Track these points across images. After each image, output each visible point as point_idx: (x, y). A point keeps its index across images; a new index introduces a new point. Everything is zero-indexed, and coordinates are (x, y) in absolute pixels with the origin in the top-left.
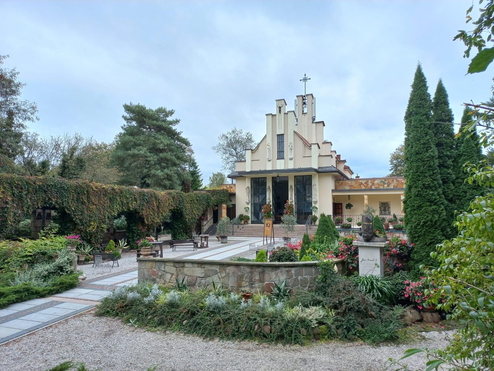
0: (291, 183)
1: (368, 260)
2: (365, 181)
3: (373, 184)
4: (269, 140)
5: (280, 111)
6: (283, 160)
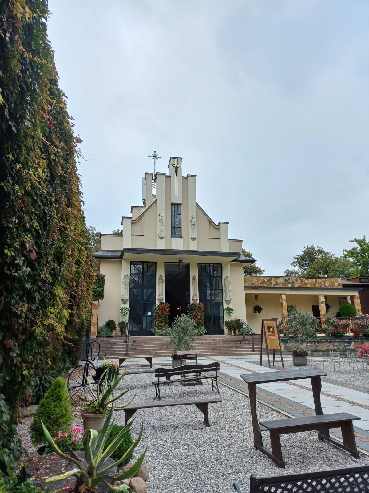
0: (194, 273)
2: (268, 279)
3: (277, 283)
5: (176, 172)
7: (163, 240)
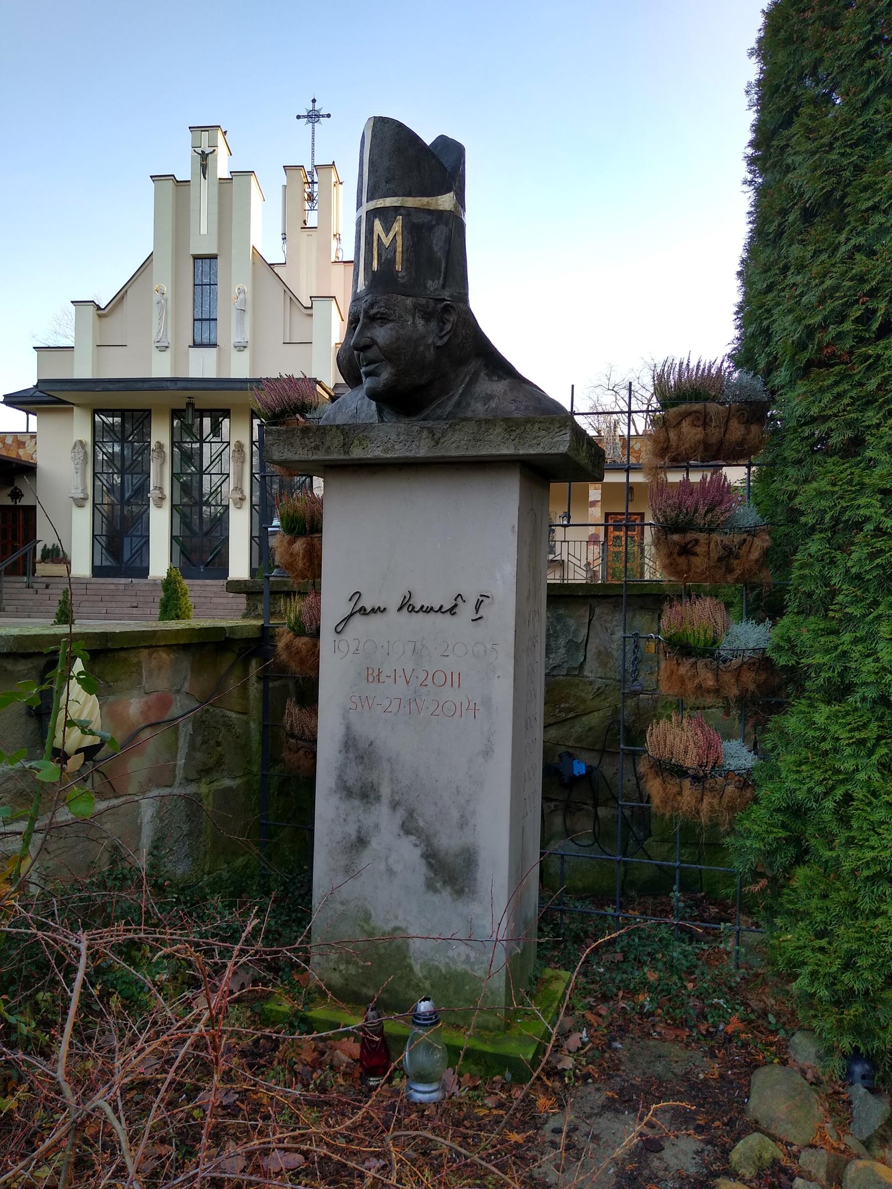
1: (407, 605)
4: (162, 279)
5: (204, 168)
6: (213, 351)
7: (168, 354)
